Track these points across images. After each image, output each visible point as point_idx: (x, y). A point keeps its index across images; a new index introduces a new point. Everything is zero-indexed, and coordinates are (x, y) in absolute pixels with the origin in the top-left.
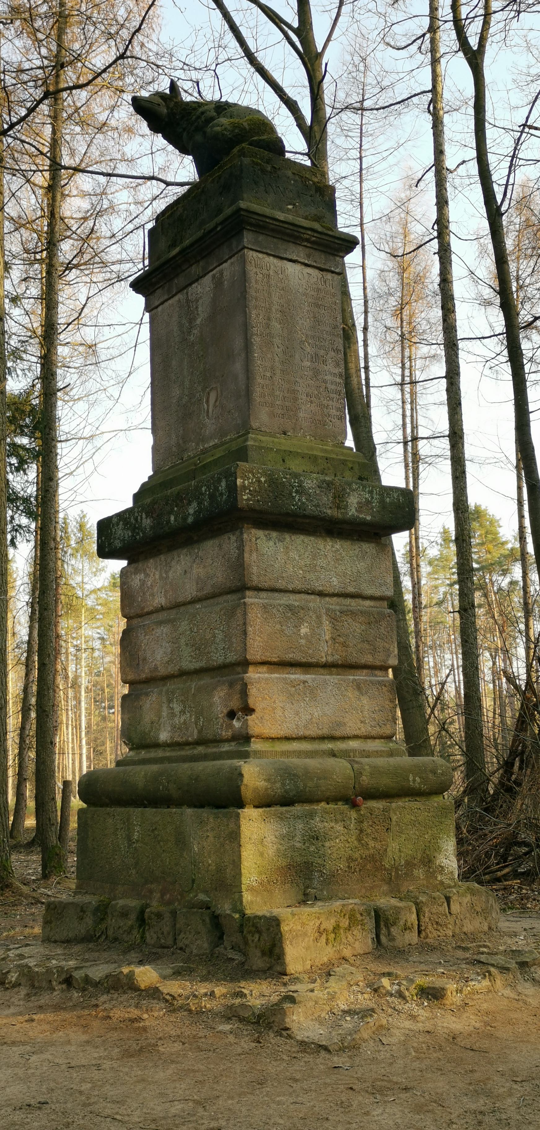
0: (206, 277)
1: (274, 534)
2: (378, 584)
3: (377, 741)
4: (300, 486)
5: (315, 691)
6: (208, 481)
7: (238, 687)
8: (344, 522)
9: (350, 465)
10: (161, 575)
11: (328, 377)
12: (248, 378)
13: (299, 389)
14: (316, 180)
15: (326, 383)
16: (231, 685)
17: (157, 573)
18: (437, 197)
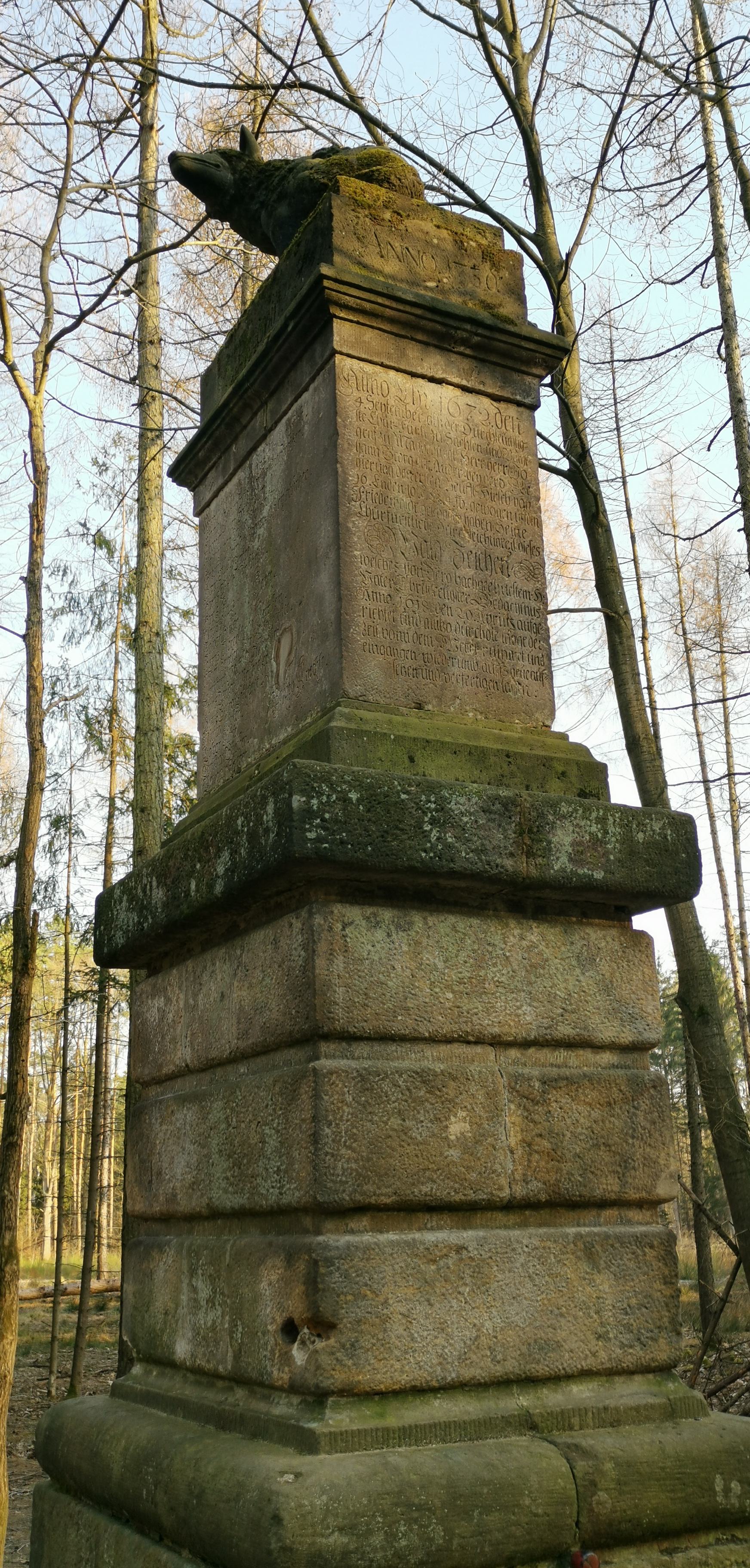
0: (277, 429)
1: (387, 915)
2: (626, 1017)
3: (638, 1378)
4: (441, 809)
5: (486, 1270)
6: (246, 805)
7: (301, 1267)
8: (542, 884)
9: (560, 769)
10: (186, 1002)
11: (513, 599)
12: (340, 599)
13: (450, 619)
14: (484, 242)
15: (509, 609)
16: (290, 1259)
17: (182, 996)
18: (738, 457)
